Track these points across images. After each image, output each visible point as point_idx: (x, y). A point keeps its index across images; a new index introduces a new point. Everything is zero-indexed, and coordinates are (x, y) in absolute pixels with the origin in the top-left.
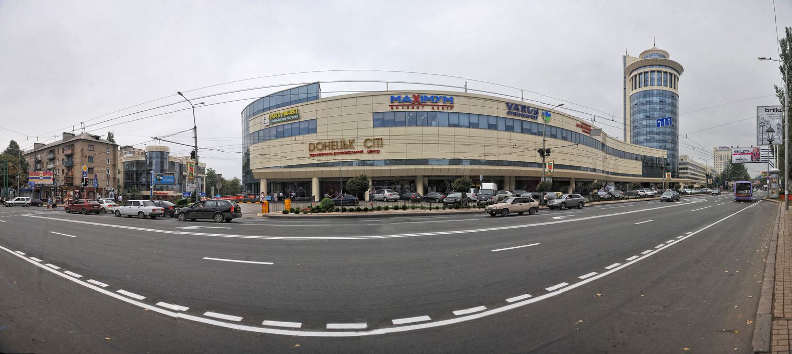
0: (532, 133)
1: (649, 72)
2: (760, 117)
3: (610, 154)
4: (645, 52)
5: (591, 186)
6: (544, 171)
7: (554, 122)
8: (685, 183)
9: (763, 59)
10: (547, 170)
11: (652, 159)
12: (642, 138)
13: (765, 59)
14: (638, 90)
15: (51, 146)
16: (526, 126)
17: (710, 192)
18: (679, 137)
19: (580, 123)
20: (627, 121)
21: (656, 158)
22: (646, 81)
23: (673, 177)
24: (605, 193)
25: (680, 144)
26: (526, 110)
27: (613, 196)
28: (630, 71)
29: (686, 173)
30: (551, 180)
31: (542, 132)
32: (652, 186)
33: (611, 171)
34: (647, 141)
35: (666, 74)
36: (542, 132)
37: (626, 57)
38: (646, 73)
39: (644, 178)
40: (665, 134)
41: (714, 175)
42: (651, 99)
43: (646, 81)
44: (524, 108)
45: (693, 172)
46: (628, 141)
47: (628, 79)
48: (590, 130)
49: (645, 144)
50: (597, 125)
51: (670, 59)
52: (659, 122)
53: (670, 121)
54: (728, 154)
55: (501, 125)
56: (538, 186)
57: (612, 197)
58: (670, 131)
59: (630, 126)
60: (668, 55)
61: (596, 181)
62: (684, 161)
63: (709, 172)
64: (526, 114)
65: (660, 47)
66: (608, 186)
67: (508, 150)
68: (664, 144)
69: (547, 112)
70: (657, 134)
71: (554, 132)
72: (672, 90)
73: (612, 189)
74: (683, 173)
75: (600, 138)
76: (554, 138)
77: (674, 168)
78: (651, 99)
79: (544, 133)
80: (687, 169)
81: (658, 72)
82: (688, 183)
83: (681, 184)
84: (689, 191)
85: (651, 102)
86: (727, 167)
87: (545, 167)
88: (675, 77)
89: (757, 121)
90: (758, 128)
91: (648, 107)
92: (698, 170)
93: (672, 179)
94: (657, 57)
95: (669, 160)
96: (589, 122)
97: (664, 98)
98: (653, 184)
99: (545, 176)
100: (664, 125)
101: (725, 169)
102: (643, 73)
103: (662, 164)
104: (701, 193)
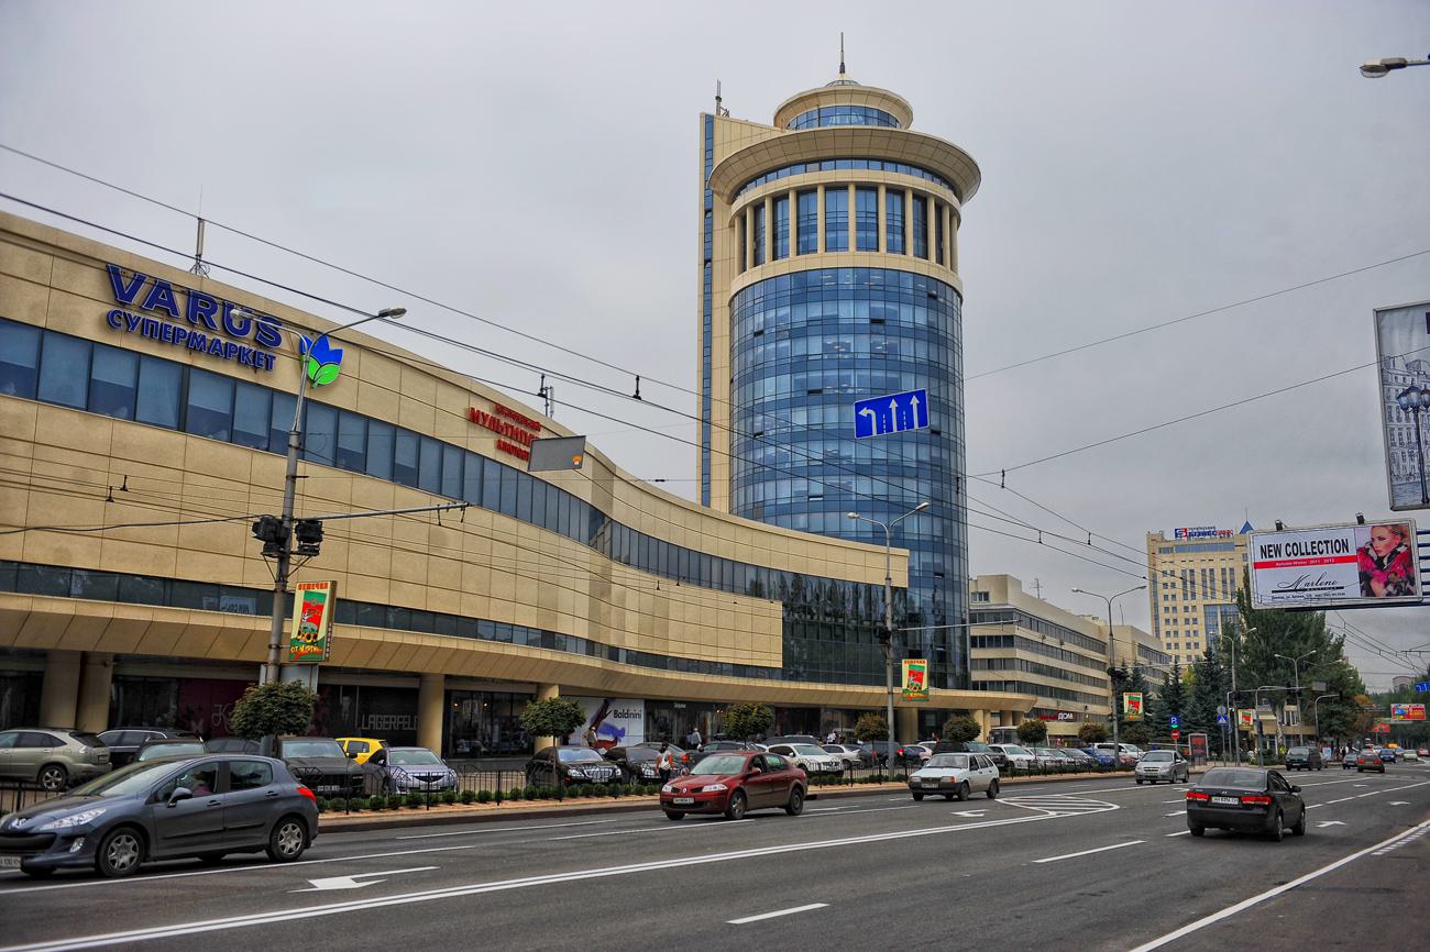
0: (234, 438)
1: (820, 191)
2: (1400, 365)
3: (628, 563)
4: (802, 100)
5: (527, 714)
6: (280, 633)
7: (349, 386)
8: (1002, 715)
9: (1388, 67)
10: (293, 627)
11: (833, 591)
12: (785, 490)
13: (1402, 65)
14: (770, 268)
15: (371, 676)
16: (204, 397)
17: (1130, 765)
18: (971, 487)
19: (485, 409)
20: (715, 406)
21: (856, 585)
22: (805, 229)
23: (939, 680)
24: (595, 756)
25: (971, 518)
26: (216, 318)
27: (632, 771)
28: (731, 187)
29: (1006, 664)
30: (310, 683)
31: (288, 435)
32: (831, 725)
33: (632, 643)
34: (808, 504)
35: (897, 199)
36: (288, 435)
37: (716, 122)
38: (805, 192)
39: (793, 685)
40: (896, 470)
41: (1154, 672)
42: (830, 310)
43: (805, 229)
44: (203, 305)
45: (1042, 660)
46: (720, 504)
47: (724, 215)
48: (530, 441)
49: (802, 520)
50: (566, 420)
51: (915, 128)
52: (864, 412)
53: (922, 407)
54: (1228, 565)
55: (61, 368)
56: (240, 708)
57: (629, 777)
58: (924, 457)
59: (731, 431)
60: (907, 111)
61: (554, 693)
62: (994, 602)
63: (1126, 655)
64: (209, 337)
65: (865, 75)
66: (609, 720)
67: (89, 511)
68: (896, 520)
69: (324, 338)
70: (859, 471)
71: (352, 442)
72: (928, 267)
73: (633, 732)
74: (990, 664)
75: (580, 484)
76: (348, 468)
77: (942, 637)
78: (830, 310)
79: (293, 441)
80: (1009, 641)
81: (861, 187)
82: (1015, 716)
83: (979, 718)
84: (1020, 755)
85: (829, 325)
86: (1228, 629)
87: (288, 612)
88: (939, 209)
89: (1384, 382)
90: (1387, 417)
91: (815, 346)
92: (1067, 647)
93: (935, 692)
94: (856, 123)
95: (920, 598)
96: (534, 406)
97: (892, 307)
98: (839, 717)
99: (283, 658)
100: (890, 429)
101: (1216, 640)
102: (792, 196)
103: (884, 616)
104: (1088, 767)
